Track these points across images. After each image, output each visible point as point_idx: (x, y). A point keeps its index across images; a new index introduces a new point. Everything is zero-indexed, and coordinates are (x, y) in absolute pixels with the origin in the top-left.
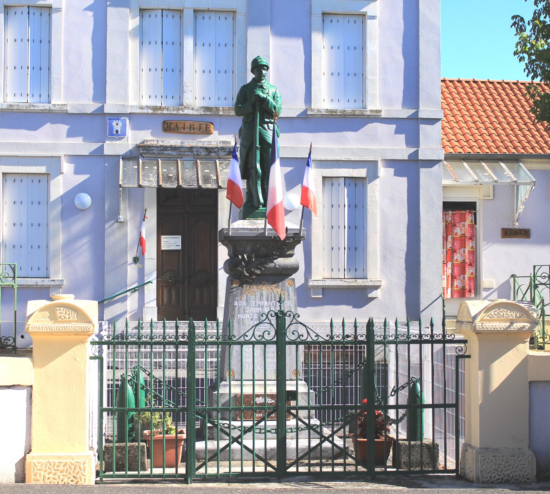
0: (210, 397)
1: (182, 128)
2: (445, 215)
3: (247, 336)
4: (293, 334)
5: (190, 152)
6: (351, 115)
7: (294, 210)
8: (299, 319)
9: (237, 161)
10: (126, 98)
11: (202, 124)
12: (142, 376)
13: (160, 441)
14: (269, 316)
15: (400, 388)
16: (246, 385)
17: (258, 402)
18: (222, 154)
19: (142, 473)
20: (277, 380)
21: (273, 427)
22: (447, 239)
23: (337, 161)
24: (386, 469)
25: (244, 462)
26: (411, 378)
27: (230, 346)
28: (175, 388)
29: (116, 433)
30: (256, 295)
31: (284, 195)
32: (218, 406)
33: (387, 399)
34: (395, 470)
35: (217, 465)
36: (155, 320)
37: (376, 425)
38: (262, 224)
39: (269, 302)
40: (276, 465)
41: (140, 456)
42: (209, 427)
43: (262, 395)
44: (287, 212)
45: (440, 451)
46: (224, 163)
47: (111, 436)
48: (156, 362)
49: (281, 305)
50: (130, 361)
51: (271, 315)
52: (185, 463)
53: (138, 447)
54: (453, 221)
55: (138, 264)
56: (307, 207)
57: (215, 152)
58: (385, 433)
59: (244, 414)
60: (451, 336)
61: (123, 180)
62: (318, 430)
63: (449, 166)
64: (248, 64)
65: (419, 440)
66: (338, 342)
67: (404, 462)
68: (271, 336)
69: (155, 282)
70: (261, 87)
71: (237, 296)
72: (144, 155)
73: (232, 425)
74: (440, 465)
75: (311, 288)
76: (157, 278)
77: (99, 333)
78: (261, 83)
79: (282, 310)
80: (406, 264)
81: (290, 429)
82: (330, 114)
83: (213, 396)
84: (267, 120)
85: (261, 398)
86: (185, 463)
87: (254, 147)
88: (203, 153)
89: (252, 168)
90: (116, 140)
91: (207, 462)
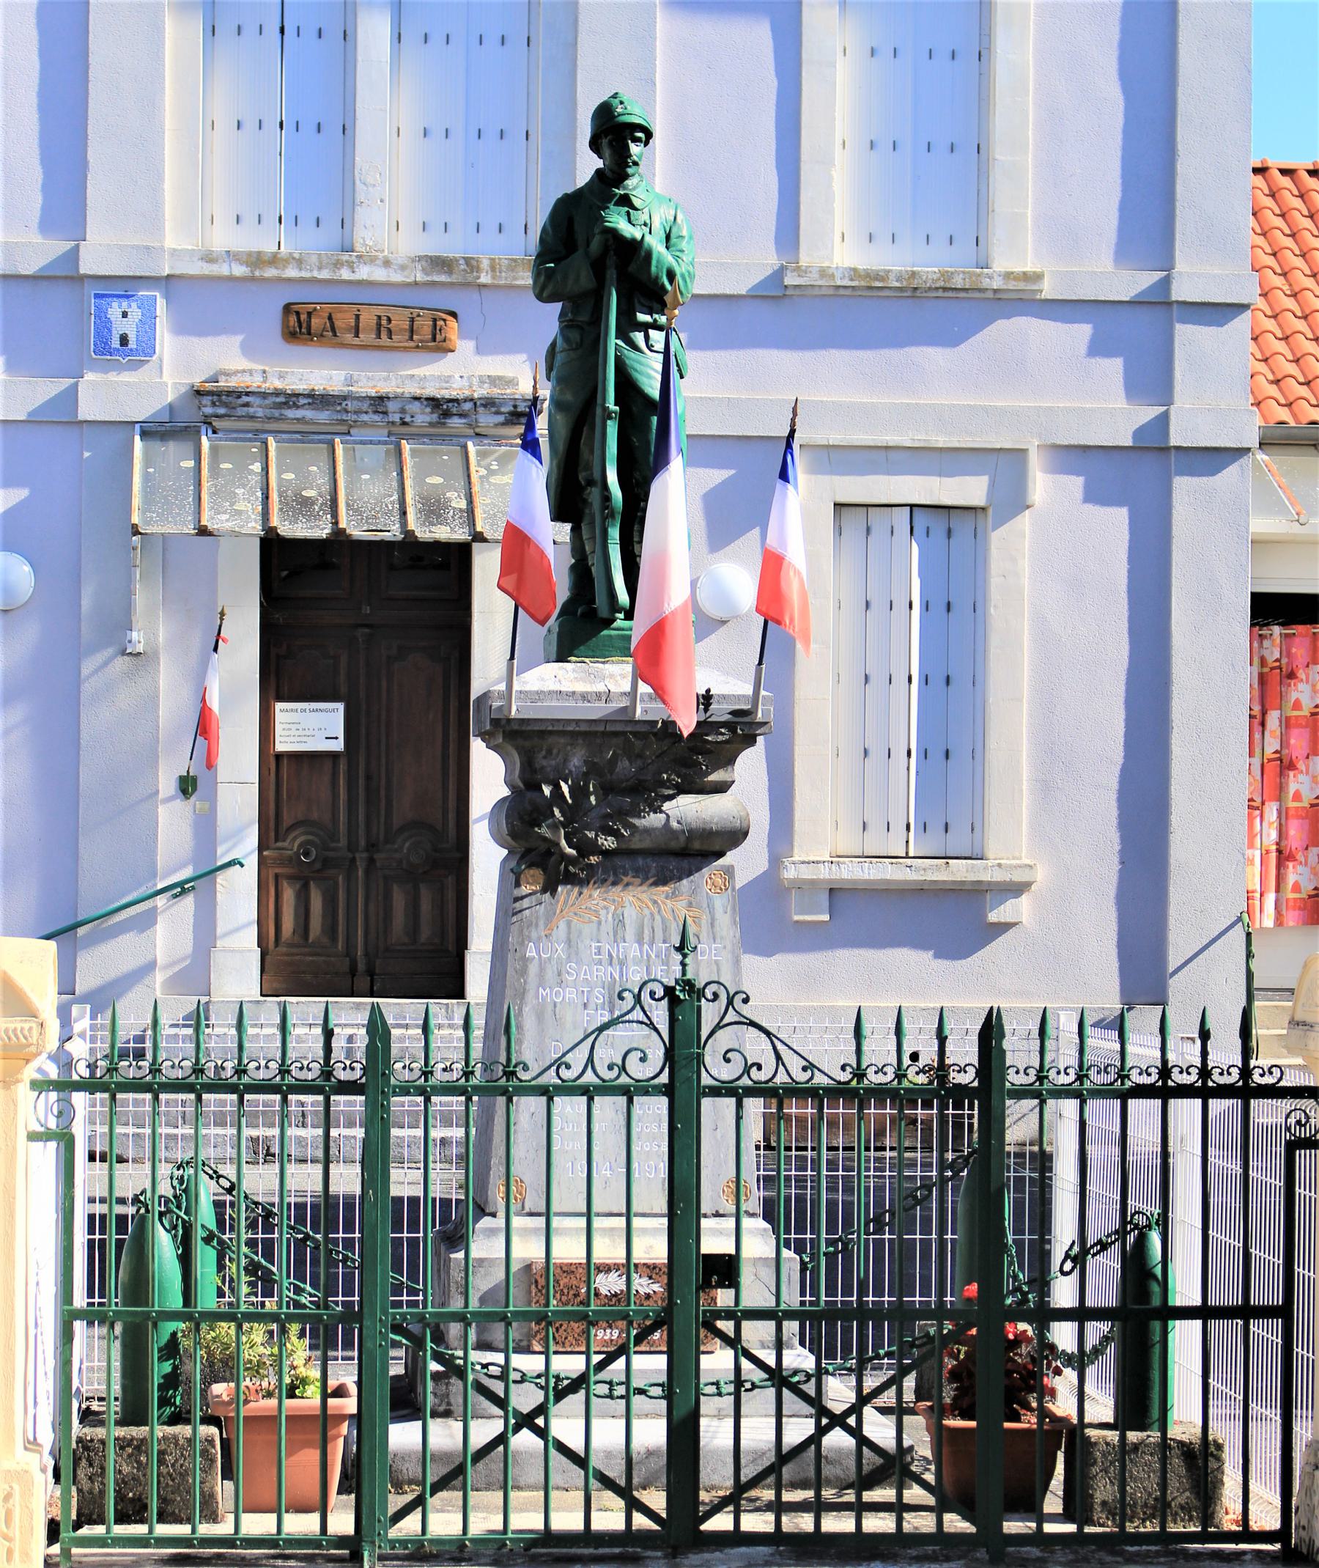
0: (439, 1271)
1: (348, 331)
2: (1258, 638)
3: (568, 1067)
4: (728, 1061)
5: (376, 412)
6: (937, 289)
7: (736, 617)
8: (746, 1010)
9: (537, 462)
10: (154, 220)
11: (419, 316)
12: (207, 1192)
13: (269, 1421)
14: (645, 997)
15: (1092, 1247)
16: (565, 1232)
17: (604, 1291)
18: (486, 420)
19: (205, 1529)
20: (671, 1215)
21: (655, 1375)
22: (1263, 724)
23: (887, 448)
24: (1040, 1527)
25: (553, 1494)
26: (1132, 1216)
27: (510, 1100)
28: (318, 1236)
29: (116, 1388)
30: (599, 923)
31: (695, 564)
32: (466, 1306)
33: (1047, 1284)
34: (1071, 1528)
35: (461, 1503)
36: (253, 993)
37: (1008, 1373)
38: (623, 676)
39: (646, 947)
40: (664, 1505)
41: (198, 1471)
42: (436, 1376)
43: (617, 1267)
44: (707, 625)
45: (1227, 1464)
46: (496, 451)
47: (100, 1399)
48: (255, 1140)
49: (687, 961)
50: (168, 1136)
51: (652, 994)
52: (353, 1496)
53: (191, 1441)
54: (1284, 661)
55: (193, 798)
56: (778, 622)
57: (461, 415)
58: (1040, 1401)
59: (557, 1330)
60: (1271, 1073)
61: (143, 511)
62: (810, 1389)
63: (1274, 468)
64: (488, 947)
65: (1156, 1425)
66: (880, 1093)
67: (1104, 1503)
68: (650, 1066)
69: (252, 862)
70: (626, 201)
71: (537, 925)
72: (216, 423)
73: (514, 1370)
74: (1227, 1513)
75: (789, 890)
76: (261, 847)
77: (61, 1047)
78: (625, 188)
79: (689, 976)
80: (1119, 808)
81: (713, 1384)
82: (863, 283)
83: (449, 1268)
84: (643, 317)
85: (613, 1276)
86: (353, 1496)
87: (599, 411)
88: (423, 417)
89: (591, 483)
90: (121, 368)
91: (428, 1496)
